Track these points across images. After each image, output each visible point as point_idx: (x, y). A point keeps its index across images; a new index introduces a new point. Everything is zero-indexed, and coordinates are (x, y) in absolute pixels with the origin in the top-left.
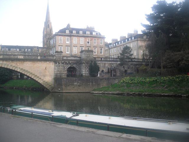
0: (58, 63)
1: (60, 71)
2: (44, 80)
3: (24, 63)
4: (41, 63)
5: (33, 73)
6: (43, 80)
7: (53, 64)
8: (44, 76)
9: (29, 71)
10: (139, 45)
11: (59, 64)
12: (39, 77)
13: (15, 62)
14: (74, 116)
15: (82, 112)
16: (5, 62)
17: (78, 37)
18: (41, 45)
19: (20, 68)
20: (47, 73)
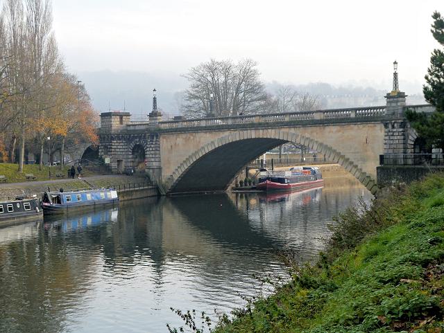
0: (390, 126)
1: (392, 146)
2: (363, 171)
3: (324, 129)
4: (356, 127)
5: (342, 154)
6: (361, 169)
7: (381, 130)
8: (364, 160)
9: (334, 148)
10: (426, 103)
11: (393, 127)
12: (348, 159)
13: (309, 129)
14: (236, 182)
15: (276, 195)
16: (292, 131)
18: (116, 191)
19: (317, 142)
20: (370, 153)
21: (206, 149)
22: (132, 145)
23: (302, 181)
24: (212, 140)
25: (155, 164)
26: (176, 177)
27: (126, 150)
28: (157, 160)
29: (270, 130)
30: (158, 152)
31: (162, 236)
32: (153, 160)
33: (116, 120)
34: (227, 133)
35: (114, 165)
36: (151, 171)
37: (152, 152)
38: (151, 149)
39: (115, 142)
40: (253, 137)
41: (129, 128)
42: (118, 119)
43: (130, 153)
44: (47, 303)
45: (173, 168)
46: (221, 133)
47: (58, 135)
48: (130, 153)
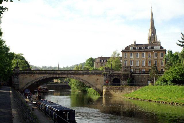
0: (106, 76)
8: (97, 85)
11: (107, 76)
16: (58, 76)
17: (140, 52)
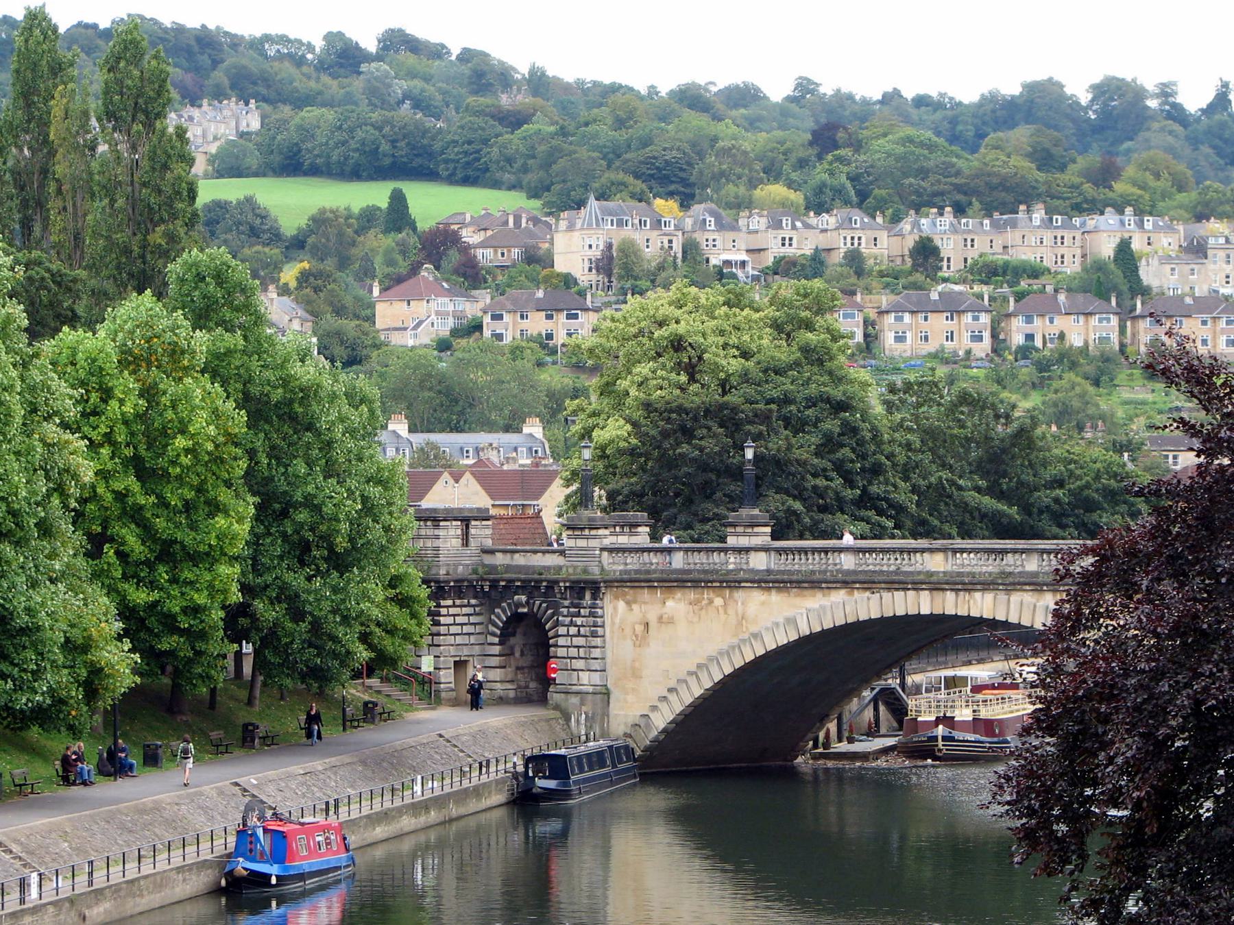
21: (704, 676)
22: (501, 615)
23: (741, 768)
24: (789, 613)
25: (587, 680)
26: (661, 720)
27: (478, 629)
28: (596, 665)
29: (978, 595)
30: (598, 641)
31: (606, 897)
32: (579, 664)
33: (452, 532)
34: (839, 596)
35: (447, 677)
36: (574, 700)
37: (580, 641)
38: (573, 630)
39: (450, 602)
40: (925, 610)
41: (488, 560)
42: (452, 531)
43: (496, 640)
44: (962, 413)
45: (651, 689)
46: (819, 595)
47: (348, 652)
48: (496, 640)
